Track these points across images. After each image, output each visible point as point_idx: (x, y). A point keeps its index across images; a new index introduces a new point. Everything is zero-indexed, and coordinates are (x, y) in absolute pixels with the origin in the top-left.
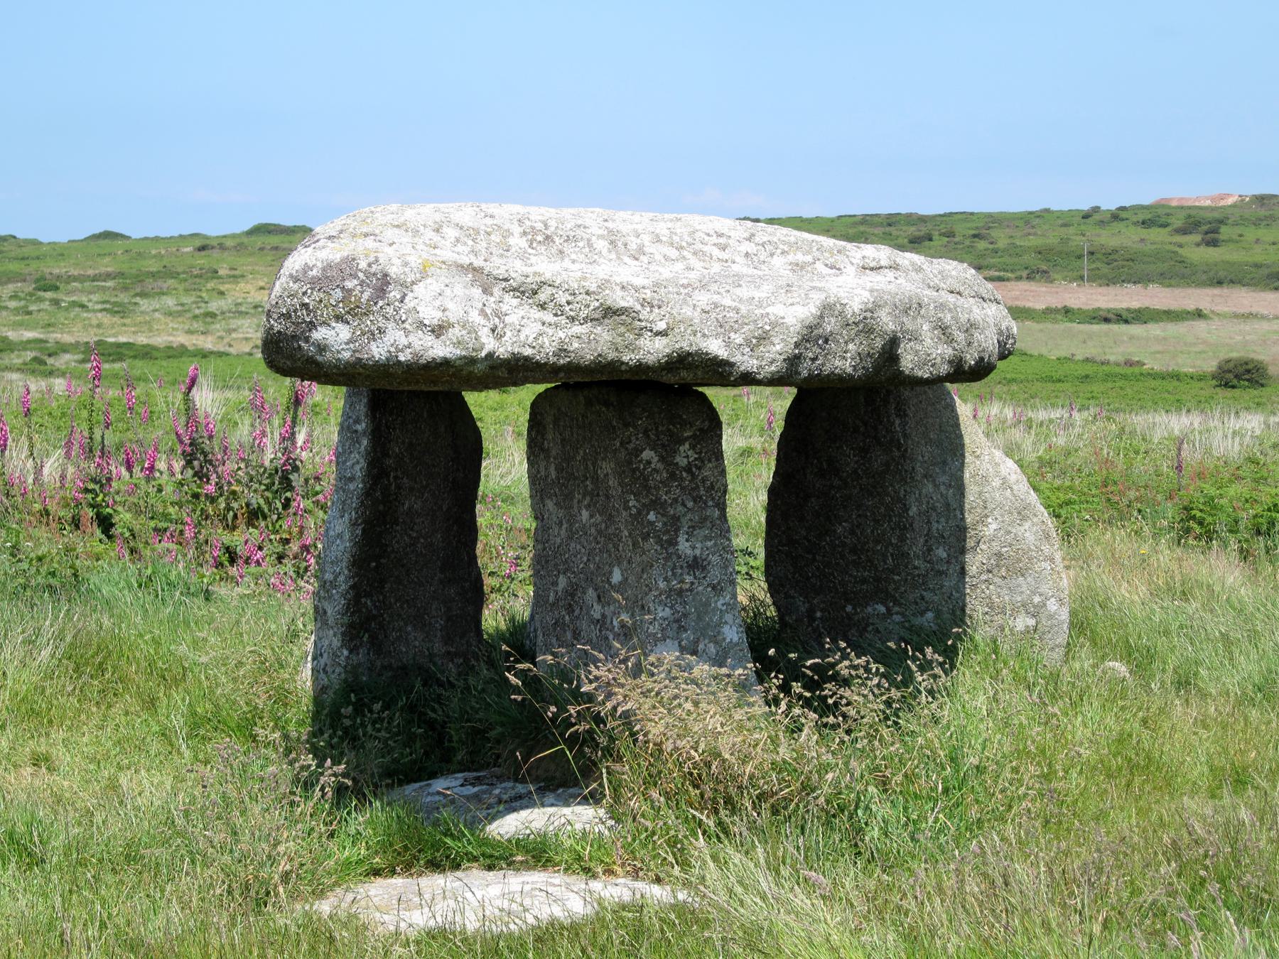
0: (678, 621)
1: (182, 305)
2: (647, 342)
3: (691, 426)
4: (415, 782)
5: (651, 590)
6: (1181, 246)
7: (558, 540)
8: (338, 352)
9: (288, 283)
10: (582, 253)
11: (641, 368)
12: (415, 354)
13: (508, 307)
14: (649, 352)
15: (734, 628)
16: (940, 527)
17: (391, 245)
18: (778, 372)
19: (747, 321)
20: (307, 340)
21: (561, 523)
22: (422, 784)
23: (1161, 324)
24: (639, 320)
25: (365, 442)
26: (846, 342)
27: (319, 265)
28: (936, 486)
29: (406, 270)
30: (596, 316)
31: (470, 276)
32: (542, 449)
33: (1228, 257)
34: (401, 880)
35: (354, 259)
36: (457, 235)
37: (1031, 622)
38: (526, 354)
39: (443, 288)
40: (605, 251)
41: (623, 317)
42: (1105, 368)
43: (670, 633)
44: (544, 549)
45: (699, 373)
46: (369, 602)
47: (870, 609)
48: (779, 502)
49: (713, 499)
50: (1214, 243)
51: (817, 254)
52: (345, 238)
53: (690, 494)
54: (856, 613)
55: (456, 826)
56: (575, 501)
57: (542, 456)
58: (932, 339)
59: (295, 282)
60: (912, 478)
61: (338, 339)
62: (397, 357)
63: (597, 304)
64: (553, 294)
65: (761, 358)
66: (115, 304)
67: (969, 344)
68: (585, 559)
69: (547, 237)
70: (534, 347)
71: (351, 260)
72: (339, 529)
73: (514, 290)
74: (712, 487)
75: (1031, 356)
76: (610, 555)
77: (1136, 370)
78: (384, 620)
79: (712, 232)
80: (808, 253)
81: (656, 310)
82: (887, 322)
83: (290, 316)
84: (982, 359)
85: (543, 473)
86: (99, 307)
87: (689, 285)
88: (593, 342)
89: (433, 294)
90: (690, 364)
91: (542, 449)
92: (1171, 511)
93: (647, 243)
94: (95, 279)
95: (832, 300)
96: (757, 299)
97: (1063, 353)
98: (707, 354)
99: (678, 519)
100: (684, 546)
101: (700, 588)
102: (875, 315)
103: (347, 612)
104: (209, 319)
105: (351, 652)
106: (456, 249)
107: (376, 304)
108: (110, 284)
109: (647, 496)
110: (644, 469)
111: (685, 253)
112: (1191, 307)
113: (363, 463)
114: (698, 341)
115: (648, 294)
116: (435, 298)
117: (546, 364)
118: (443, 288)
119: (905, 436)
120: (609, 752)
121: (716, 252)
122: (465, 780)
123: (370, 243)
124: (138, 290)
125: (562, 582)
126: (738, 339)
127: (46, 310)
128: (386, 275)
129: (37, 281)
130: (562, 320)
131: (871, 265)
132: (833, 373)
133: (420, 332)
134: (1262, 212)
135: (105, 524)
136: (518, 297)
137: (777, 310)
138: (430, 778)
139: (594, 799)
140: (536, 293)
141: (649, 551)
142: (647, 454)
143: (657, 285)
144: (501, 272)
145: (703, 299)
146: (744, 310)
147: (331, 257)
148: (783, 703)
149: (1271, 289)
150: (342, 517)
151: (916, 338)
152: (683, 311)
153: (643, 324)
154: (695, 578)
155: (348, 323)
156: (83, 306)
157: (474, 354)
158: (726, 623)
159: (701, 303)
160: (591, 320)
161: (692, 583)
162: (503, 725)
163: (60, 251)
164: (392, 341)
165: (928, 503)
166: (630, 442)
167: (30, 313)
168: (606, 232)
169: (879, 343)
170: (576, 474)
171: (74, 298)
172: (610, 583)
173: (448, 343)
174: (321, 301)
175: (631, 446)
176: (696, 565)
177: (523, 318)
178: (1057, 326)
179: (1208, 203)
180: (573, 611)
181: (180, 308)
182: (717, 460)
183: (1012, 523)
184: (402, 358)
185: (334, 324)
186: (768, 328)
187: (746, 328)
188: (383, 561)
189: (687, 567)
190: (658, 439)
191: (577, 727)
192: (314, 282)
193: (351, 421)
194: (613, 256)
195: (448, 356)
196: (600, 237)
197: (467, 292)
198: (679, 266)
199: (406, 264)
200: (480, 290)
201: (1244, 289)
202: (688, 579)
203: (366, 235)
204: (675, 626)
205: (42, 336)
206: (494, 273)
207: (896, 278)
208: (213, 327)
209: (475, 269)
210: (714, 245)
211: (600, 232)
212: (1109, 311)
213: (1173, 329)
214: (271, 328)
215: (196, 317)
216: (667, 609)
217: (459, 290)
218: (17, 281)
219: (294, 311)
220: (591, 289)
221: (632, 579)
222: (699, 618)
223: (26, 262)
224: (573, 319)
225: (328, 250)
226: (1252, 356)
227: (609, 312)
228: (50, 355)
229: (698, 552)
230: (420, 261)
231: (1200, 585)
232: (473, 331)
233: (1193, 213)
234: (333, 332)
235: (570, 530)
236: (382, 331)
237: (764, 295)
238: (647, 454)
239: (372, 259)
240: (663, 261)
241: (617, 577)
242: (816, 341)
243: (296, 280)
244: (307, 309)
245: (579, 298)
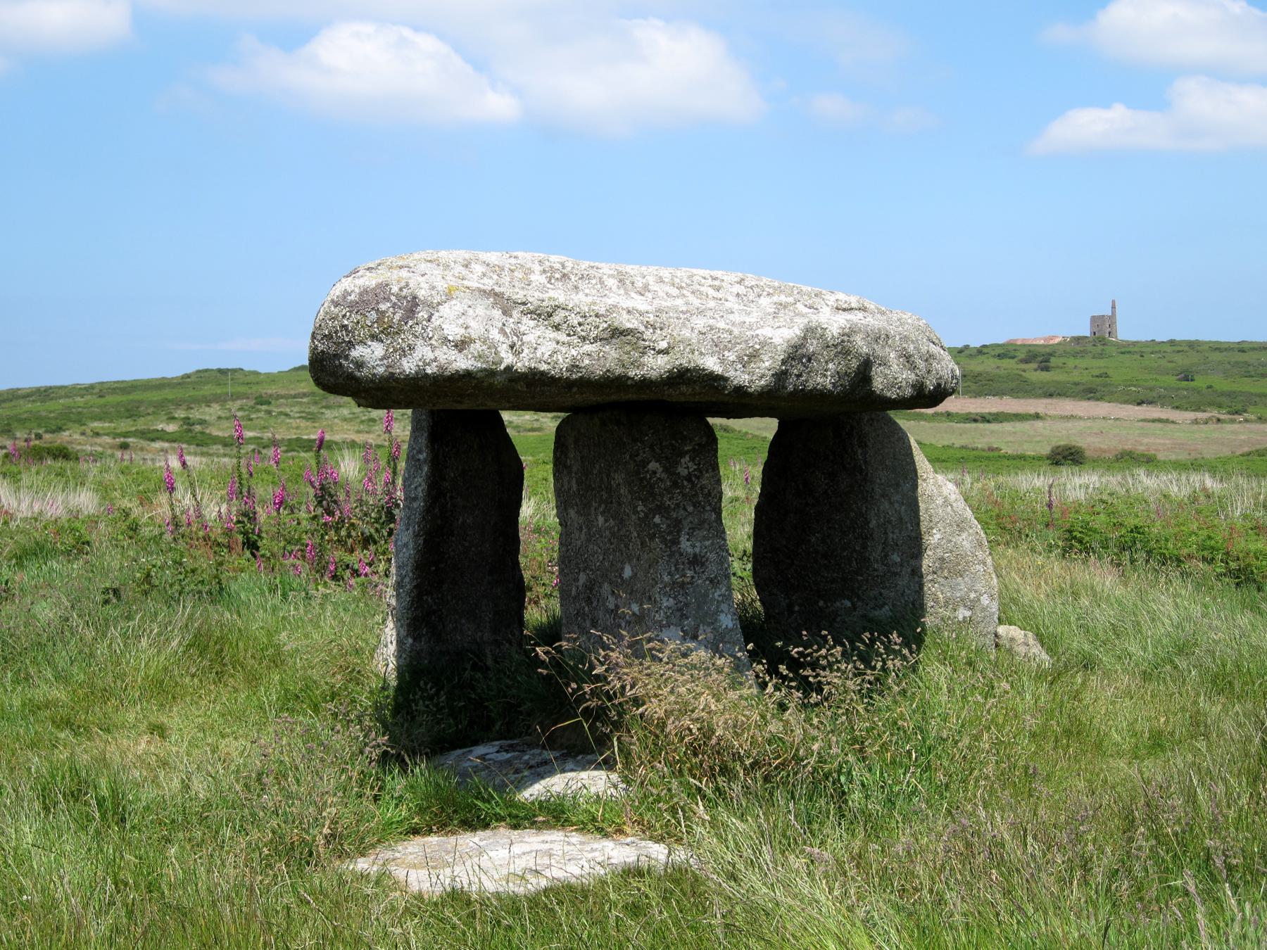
0: (680, 610)
1: (354, 413)
2: (650, 359)
3: (691, 442)
4: (460, 748)
5: (657, 583)
6: (1024, 371)
7: (579, 543)
8: (374, 368)
9: (329, 307)
10: (594, 289)
11: (645, 383)
12: (440, 367)
13: (525, 328)
14: (652, 368)
15: (729, 616)
16: (895, 537)
17: (423, 275)
18: (767, 386)
19: (739, 341)
20: (346, 358)
22: (465, 750)
23: (1012, 423)
24: (644, 340)
25: (426, 469)
26: (826, 362)
27: (357, 290)
28: (891, 503)
29: (433, 292)
30: (605, 336)
31: (492, 300)
32: (565, 467)
33: (1056, 378)
34: (437, 839)
35: (387, 285)
36: (484, 270)
37: (968, 614)
38: (542, 369)
39: (466, 308)
40: (614, 288)
41: (629, 337)
42: (974, 452)
43: (674, 621)
44: (568, 550)
45: (697, 388)
46: (429, 599)
47: (838, 604)
48: (764, 518)
49: (710, 504)
50: (1047, 369)
51: (798, 297)
52: (382, 270)
53: (690, 500)
54: (827, 607)
55: (486, 790)
56: (593, 509)
57: (565, 472)
58: (898, 365)
59: (335, 307)
60: (872, 497)
61: (373, 356)
62: (424, 370)
63: (605, 325)
64: (566, 317)
65: (751, 373)
66: (309, 413)
67: (929, 372)
68: (601, 558)
69: (564, 275)
70: (549, 363)
71: (384, 286)
72: (405, 540)
73: (531, 313)
74: (709, 494)
75: (925, 445)
76: (622, 554)
77: (996, 454)
78: (442, 613)
79: (708, 276)
80: (790, 295)
81: (658, 331)
82: (862, 346)
83: (332, 337)
84: (939, 385)
85: (566, 487)
86: (298, 415)
87: (687, 311)
89: (456, 313)
90: (688, 379)
91: (565, 467)
92: (1053, 536)
93: (651, 283)
94: (295, 397)
95: (813, 324)
96: (748, 323)
97: (946, 443)
98: (704, 370)
99: (680, 521)
100: (685, 545)
101: (700, 582)
102: (852, 339)
103: (411, 608)
104: (371, 423)
105: (415, 639)
106: (482, 281)
107: (406, 323)
108: (305, 400)
111: (685, 292)
112: (1032, 411)
113: (424, 486)
114: (695, 358)
115: (651, 318)
116: (458, 317)
117: (560, 378)
118: (466, 308)
119: (866, 462)
120: (617, 726)
121: (711, 292)
122: (501, 747)
123: (404, 273)
124: (324, 404)
125: (583, 578)
126: (731, 356)
127: (262, 418)
128: (415, 298)
129: (256, 398)
130: (575, 340)
131: (844, 307)
132: (815, 388)
133: (445, 347)
134: (1078, 348)
135: (252, 546)
136: (535, 319)
137: (765, 332)
138: (472, 746)
139: (608, 765)
140: (551, 316)
141: (655, 549)
142: (653, 465)
143: (659, 311)
144: (519, 296)
145: (700, 323)
146: (736, 331)
147: (367, 283)
148: (770, 684)
149: (1085, 399)
150: (407, 530)
151: (884, 363)
152: (683, 333)
153: (647, 343)
154: (695, 572)
155: (382, 341)
156: (287, 415)
157: (494, 367)
158: (722, 611)
159: (698, 326)
160: (601, 340)
161: (693, 577)
162: (532, 701)
163: (272, 378)
164: (420, 356)
165: (885, 517)
167: (251, 420)
168: (616, 273)
169: (855, 364)
170: (593, 486)
171: (282, 410)
172: (622, 578)
173: (470, 356)
174: (358, 322)
175: (639, 458)
176: (696, 561)
177: (539, 337)
178: (941, 424)
179: (1042, 342)
180: (592, 603)
181: (351, 416)
182: (714, 470)
183: (952, 534)
184: (429, 371)
185: (369, 343)
186: (757, 347)
187: (739, 347)
188: (442, 566)
189: (688, 563)
190: (662, 453)
191: (589, 703)
192: (353, 306)
193: (415, 451)
194: (622, 292)
195: (470, 368)
196: (610, 276)
197: (488, 312)
198: (679, 302)
199: (433, 288)
200: (500, 312)
201: (1068, 399)
202: (689, 573)
203: (401, 267)
204: (678, 614)
205: (259, 435)
206: (514, 297)
207: (865, 317)
208: (374, 428)
209: (496, 294)
210: (710, 286)
211: (611, 272)
212: (977, 414)
213: (1019, 426)
214: (316, 348)
215: (362, 422)
216: (671, 600)
217: (481, 310)
218: (243, 399)
219: (335, 333)
220: (600, 313)
221: (641, 574)
222: (699, 607)
223: (249, 386)
224: (584, 339)
225: (366, 278)
226: (1073, 443)
227: (617, 333)
228: (264, 448)
229: (697, 550)
230: (446, 286)
231: (1085, 587)
232: (493, 346)
233: (1032, 349)
234: (369, 350)
236: (411, 348)
237: (753, 320)
239: (403, 284)
240: (665, 297)
241: (628, 572)
242: (801, 361)
243: (336, 304)
244: (347, 330)
245: (589, 320)
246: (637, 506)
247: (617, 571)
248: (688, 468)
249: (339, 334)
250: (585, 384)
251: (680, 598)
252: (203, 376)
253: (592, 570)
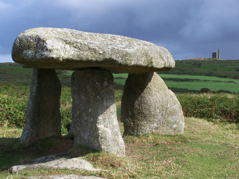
21: (78, 100)
25: (36, 85)
49: (112, 94)
73: (68, 43)
125: (78, 112)
142: (97, 83)
238: (97, 83)
241: (90, 110)
250: (81, 62)
251: (104, 117)
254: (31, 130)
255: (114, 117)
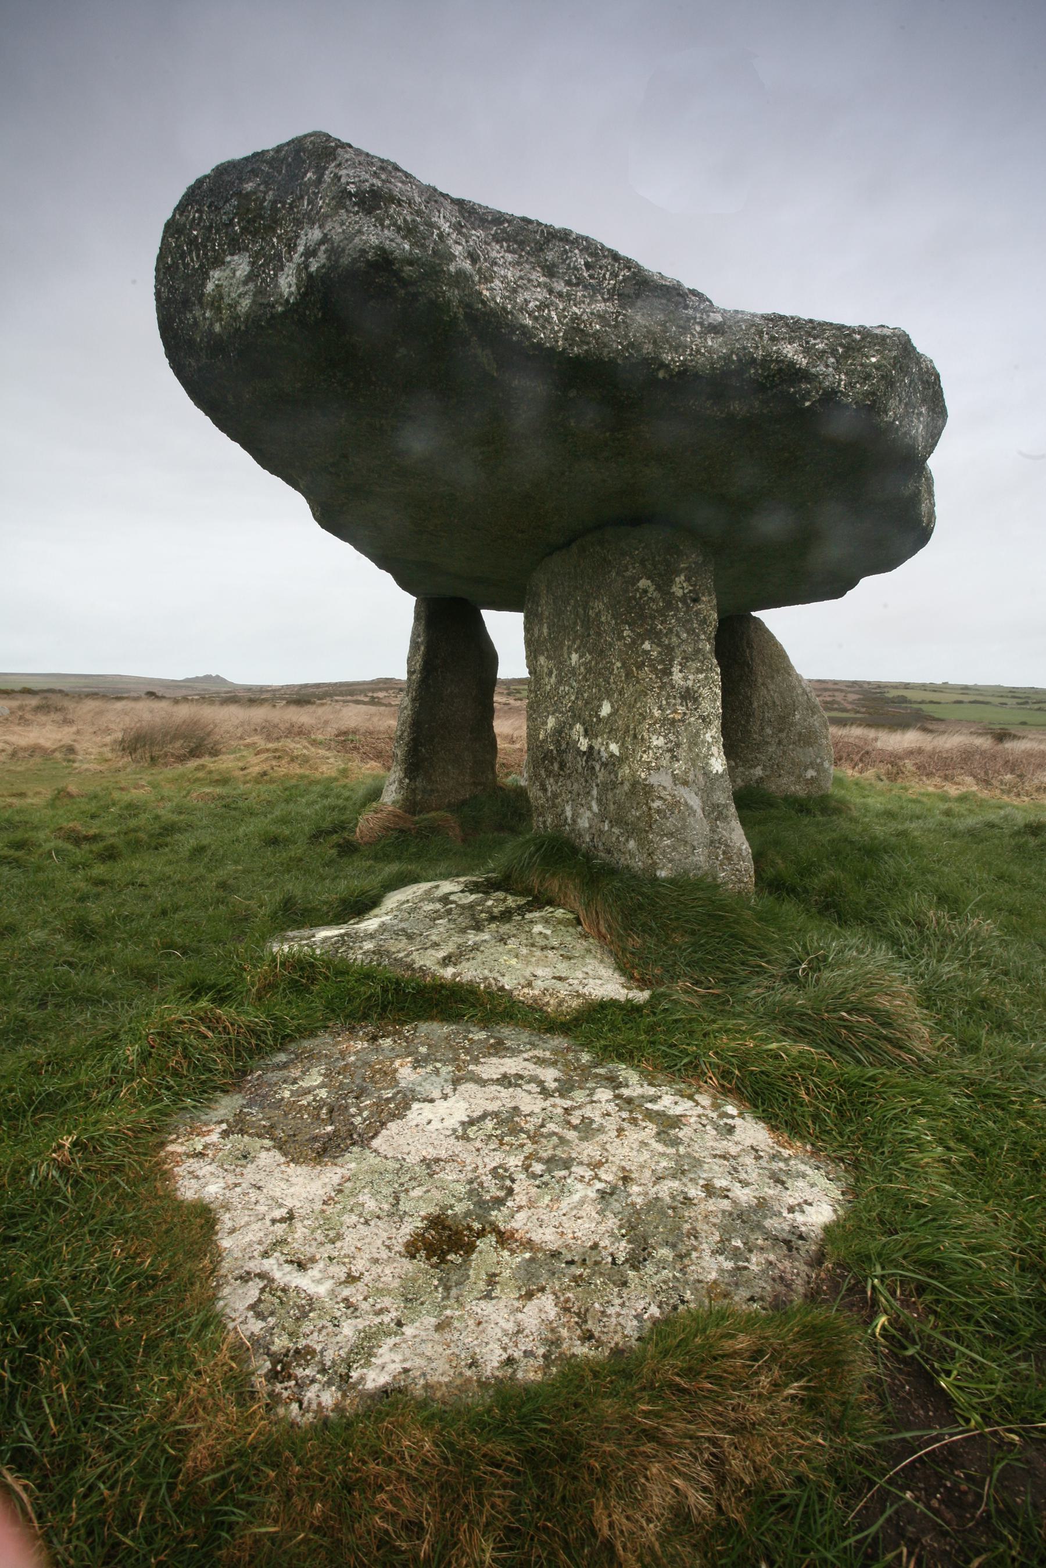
0: (671, 750)
5: (644, 718)
7: (548, 688)
25: (422, 648)
28: (768, 691)
32: (536, 615)
49: (705, 633)
53: (683, 626)
68: (573, 698)
88: (622, 326)
91: (536, 615)
99: (673, 649)
100: (677, 676)
101: (692, 719)
109: (642, 625)
110: (641, 598)
117: (552, 349)
125: (551, 722)
141: (644, 679)
142: (644, 583)
158: (712, 755)
161: (685, 714)
166: (627, 570)
172: (598, 716)
173: (387, 222)
175: (628, 574)
202: (681, 709)
204: (668, 755)
216: (661, 738)
229: (690, 683)
235: (559, 675)
241: (606, 709)
246: (623, 631)
247: (592, 710)
248: (683, 588)
249: (188, 260)
251: (671, 737)
252: (379, 681)
253: (561, 713)
254: (407, 781)
255: (710, 740)
